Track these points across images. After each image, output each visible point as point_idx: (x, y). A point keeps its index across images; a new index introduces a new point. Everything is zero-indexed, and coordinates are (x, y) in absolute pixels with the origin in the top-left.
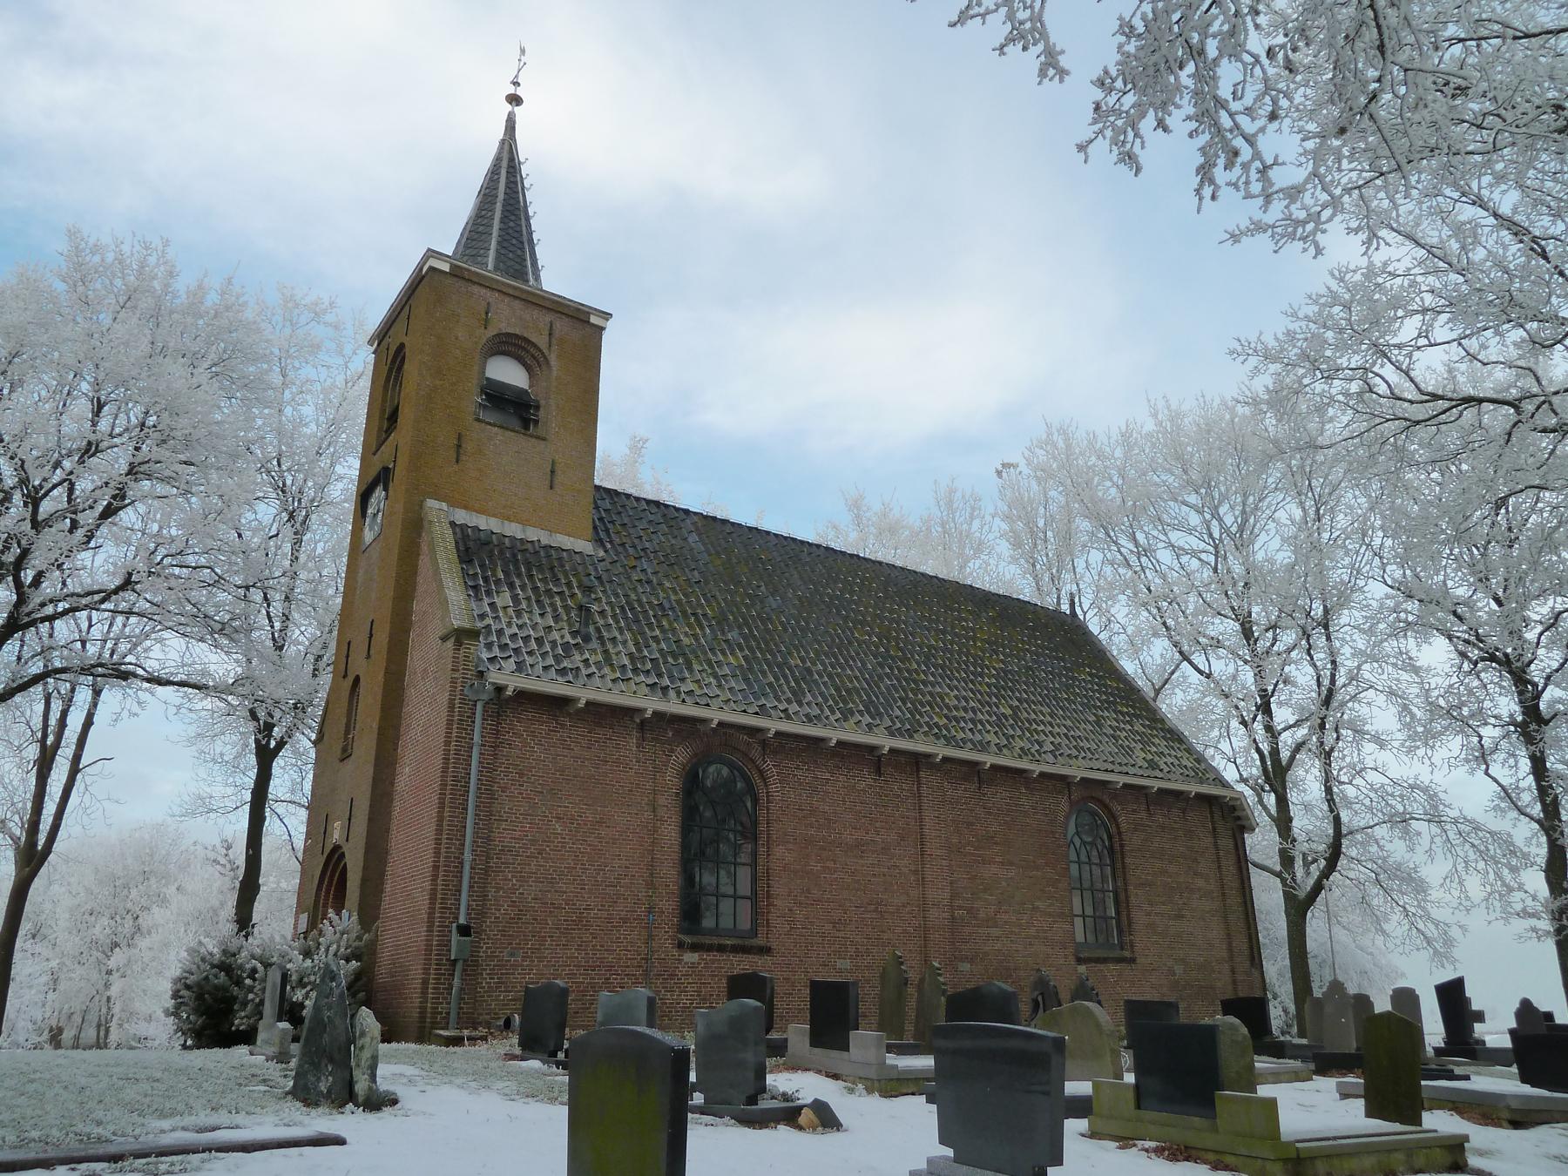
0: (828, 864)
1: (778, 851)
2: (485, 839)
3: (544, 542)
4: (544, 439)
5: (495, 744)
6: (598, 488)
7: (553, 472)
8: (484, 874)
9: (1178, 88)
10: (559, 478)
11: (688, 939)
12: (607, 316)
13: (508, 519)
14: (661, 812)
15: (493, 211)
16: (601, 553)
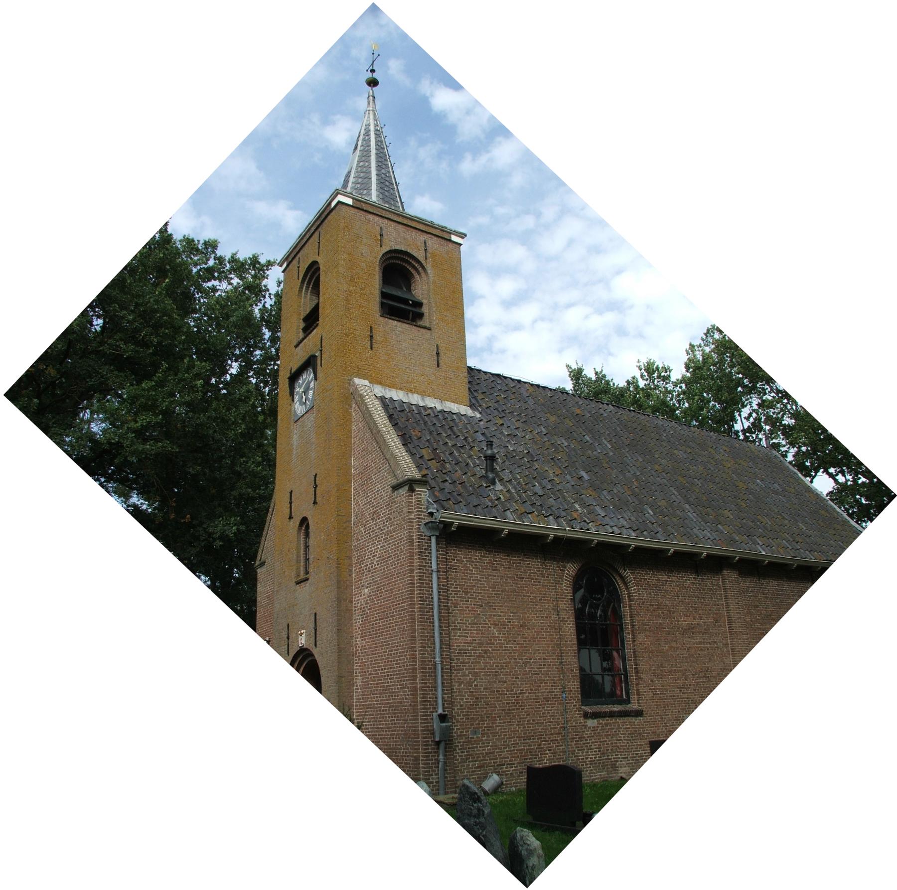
0: (674, 644)
1: (641, 638)
2: (446, 644)
3: (439, 408)
4: (429, 329)
5: (445, 570)
6: (470, 368)
7: (438, 354)
8: (449, 670)
9: (229, 262)
10: (443, 359)
11: (588, 709)
12: (463, 236)
13: (411, 391)
14: (563, 615)
15: (369, 161)
16: (478, 415)
